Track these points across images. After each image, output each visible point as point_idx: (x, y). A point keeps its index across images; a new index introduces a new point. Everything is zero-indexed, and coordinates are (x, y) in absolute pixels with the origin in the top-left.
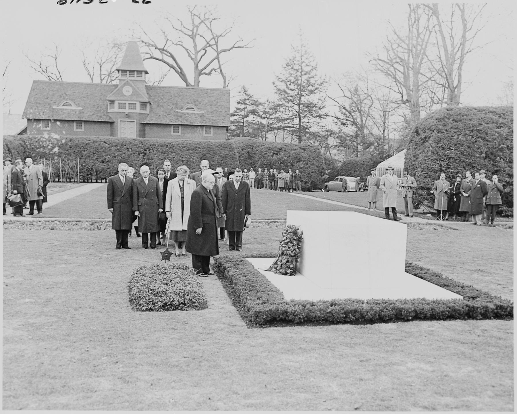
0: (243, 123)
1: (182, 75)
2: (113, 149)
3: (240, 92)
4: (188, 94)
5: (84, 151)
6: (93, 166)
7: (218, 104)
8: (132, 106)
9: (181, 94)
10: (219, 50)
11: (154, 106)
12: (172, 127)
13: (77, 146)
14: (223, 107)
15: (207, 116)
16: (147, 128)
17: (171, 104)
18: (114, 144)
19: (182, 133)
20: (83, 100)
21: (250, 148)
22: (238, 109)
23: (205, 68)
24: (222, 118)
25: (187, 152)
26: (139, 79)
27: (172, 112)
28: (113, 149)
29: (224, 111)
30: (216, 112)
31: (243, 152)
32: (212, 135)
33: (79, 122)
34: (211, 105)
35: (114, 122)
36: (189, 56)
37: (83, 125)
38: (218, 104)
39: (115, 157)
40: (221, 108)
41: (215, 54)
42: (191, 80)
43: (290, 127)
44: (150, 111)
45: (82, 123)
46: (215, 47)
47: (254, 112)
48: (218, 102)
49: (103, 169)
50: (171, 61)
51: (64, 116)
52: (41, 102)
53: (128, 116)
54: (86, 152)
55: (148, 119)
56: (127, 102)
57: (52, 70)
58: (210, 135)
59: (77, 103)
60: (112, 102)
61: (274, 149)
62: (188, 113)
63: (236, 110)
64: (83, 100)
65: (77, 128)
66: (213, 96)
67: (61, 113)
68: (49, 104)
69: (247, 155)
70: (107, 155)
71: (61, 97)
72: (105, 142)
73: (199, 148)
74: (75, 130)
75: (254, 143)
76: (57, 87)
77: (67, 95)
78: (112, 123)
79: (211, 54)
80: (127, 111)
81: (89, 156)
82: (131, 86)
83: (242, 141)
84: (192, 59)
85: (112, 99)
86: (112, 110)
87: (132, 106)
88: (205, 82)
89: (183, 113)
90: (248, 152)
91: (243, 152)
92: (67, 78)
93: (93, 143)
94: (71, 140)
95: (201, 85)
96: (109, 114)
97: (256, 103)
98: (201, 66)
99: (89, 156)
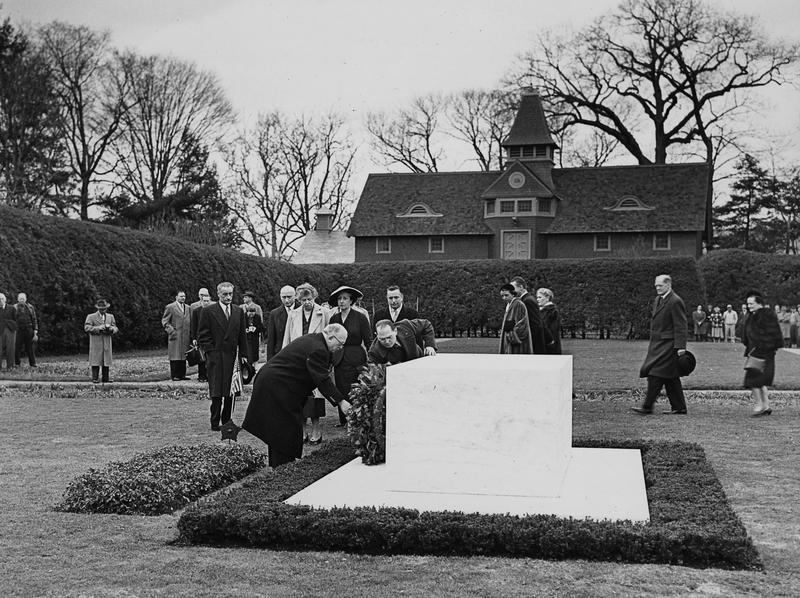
0: (748, 224)
1: (633, 147)
2: (478, 279)
3: (740, 168)
4: (627, 179)
5: (431, 285)
6: (444, 309)
7: (684, 192)
8: (525, 206)
9: (614, 178)
10: (699, 98)
11: (565, 202)
12: (655, 239)
13: (421, 276)
14: (692, 196)
15: (659, 214)
16: (551, 244)
17: (594, 199)
18: (480, 272)
19: (612, 249)
20: (446, 201)
21: (736, 268)
22: (735, 198)
23: (676, 130)
24: (690, 216)
25: (606, 279)
26: (528, 159)
27: (596, 212)
28: (478, 279)
29: (693, 203)
30: (679, 207)
31: (722, 276)
32: (669, 248)
33: (437, 239)
34: (669, 195)
35: (493, 235)
36: (648, 110)
37: (655, 239)
38: (684, 192)
39: (481, 293)
40: (688, 198)
41: (691, 107)
42: (648, 149)
43: (274, 238)
44: (557, 213)
45: (667, 237)
46: (689, 91)
47: (767, 202)
48: (682, 188)
49: (460, 314)
50: (612, 125)
51: (412, 230)
52: (378, 209)
53: (517, 223)
54: (433, 287)
55: (552, 226)
56: (516, 200)
57: (421, 155)
58: (665, 249)
59: (434, 207)
60: (491, 201)
61: (786, 268)
62: (624, 212)
63: (731, 200)
64: (446, 201)
65: (598, 247)
66: (674, 179)
67: (408, 225)
68: (391, 211)
69: (729, 282)
70: (468, 291)
71: (410, 199)
72: (465, 269)
73: (628, 272)
74: (595, 249)
75: (744, 258)
76: (406, 182)
77: (419, 194)
78: (490, 238)
79: (685, 105)
80: (515, 214)
81: (439, 294)
82: (524, 172)
83: (718, 257)
84: (652, 116)
85: (490, 195)
86: (491, 215)
87: (525, 206)
88: (676, 155)
89: (615, 213)
90: (732, 276)
91: (722, 276)
92: (443, 167)
93: (447, 270)
94: (412, 268)
95: (668, 161)
96: (486, 222)
97: (774, 185)
98: (668, 128)
99: (439, 294)
